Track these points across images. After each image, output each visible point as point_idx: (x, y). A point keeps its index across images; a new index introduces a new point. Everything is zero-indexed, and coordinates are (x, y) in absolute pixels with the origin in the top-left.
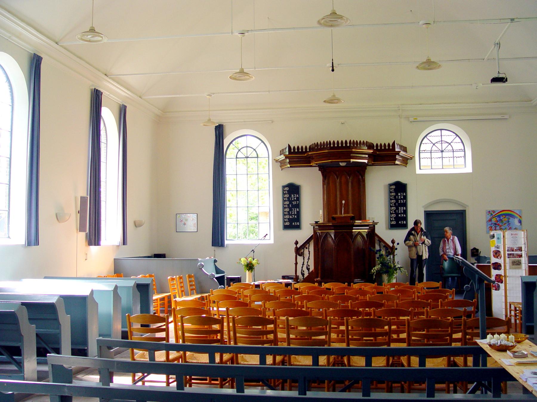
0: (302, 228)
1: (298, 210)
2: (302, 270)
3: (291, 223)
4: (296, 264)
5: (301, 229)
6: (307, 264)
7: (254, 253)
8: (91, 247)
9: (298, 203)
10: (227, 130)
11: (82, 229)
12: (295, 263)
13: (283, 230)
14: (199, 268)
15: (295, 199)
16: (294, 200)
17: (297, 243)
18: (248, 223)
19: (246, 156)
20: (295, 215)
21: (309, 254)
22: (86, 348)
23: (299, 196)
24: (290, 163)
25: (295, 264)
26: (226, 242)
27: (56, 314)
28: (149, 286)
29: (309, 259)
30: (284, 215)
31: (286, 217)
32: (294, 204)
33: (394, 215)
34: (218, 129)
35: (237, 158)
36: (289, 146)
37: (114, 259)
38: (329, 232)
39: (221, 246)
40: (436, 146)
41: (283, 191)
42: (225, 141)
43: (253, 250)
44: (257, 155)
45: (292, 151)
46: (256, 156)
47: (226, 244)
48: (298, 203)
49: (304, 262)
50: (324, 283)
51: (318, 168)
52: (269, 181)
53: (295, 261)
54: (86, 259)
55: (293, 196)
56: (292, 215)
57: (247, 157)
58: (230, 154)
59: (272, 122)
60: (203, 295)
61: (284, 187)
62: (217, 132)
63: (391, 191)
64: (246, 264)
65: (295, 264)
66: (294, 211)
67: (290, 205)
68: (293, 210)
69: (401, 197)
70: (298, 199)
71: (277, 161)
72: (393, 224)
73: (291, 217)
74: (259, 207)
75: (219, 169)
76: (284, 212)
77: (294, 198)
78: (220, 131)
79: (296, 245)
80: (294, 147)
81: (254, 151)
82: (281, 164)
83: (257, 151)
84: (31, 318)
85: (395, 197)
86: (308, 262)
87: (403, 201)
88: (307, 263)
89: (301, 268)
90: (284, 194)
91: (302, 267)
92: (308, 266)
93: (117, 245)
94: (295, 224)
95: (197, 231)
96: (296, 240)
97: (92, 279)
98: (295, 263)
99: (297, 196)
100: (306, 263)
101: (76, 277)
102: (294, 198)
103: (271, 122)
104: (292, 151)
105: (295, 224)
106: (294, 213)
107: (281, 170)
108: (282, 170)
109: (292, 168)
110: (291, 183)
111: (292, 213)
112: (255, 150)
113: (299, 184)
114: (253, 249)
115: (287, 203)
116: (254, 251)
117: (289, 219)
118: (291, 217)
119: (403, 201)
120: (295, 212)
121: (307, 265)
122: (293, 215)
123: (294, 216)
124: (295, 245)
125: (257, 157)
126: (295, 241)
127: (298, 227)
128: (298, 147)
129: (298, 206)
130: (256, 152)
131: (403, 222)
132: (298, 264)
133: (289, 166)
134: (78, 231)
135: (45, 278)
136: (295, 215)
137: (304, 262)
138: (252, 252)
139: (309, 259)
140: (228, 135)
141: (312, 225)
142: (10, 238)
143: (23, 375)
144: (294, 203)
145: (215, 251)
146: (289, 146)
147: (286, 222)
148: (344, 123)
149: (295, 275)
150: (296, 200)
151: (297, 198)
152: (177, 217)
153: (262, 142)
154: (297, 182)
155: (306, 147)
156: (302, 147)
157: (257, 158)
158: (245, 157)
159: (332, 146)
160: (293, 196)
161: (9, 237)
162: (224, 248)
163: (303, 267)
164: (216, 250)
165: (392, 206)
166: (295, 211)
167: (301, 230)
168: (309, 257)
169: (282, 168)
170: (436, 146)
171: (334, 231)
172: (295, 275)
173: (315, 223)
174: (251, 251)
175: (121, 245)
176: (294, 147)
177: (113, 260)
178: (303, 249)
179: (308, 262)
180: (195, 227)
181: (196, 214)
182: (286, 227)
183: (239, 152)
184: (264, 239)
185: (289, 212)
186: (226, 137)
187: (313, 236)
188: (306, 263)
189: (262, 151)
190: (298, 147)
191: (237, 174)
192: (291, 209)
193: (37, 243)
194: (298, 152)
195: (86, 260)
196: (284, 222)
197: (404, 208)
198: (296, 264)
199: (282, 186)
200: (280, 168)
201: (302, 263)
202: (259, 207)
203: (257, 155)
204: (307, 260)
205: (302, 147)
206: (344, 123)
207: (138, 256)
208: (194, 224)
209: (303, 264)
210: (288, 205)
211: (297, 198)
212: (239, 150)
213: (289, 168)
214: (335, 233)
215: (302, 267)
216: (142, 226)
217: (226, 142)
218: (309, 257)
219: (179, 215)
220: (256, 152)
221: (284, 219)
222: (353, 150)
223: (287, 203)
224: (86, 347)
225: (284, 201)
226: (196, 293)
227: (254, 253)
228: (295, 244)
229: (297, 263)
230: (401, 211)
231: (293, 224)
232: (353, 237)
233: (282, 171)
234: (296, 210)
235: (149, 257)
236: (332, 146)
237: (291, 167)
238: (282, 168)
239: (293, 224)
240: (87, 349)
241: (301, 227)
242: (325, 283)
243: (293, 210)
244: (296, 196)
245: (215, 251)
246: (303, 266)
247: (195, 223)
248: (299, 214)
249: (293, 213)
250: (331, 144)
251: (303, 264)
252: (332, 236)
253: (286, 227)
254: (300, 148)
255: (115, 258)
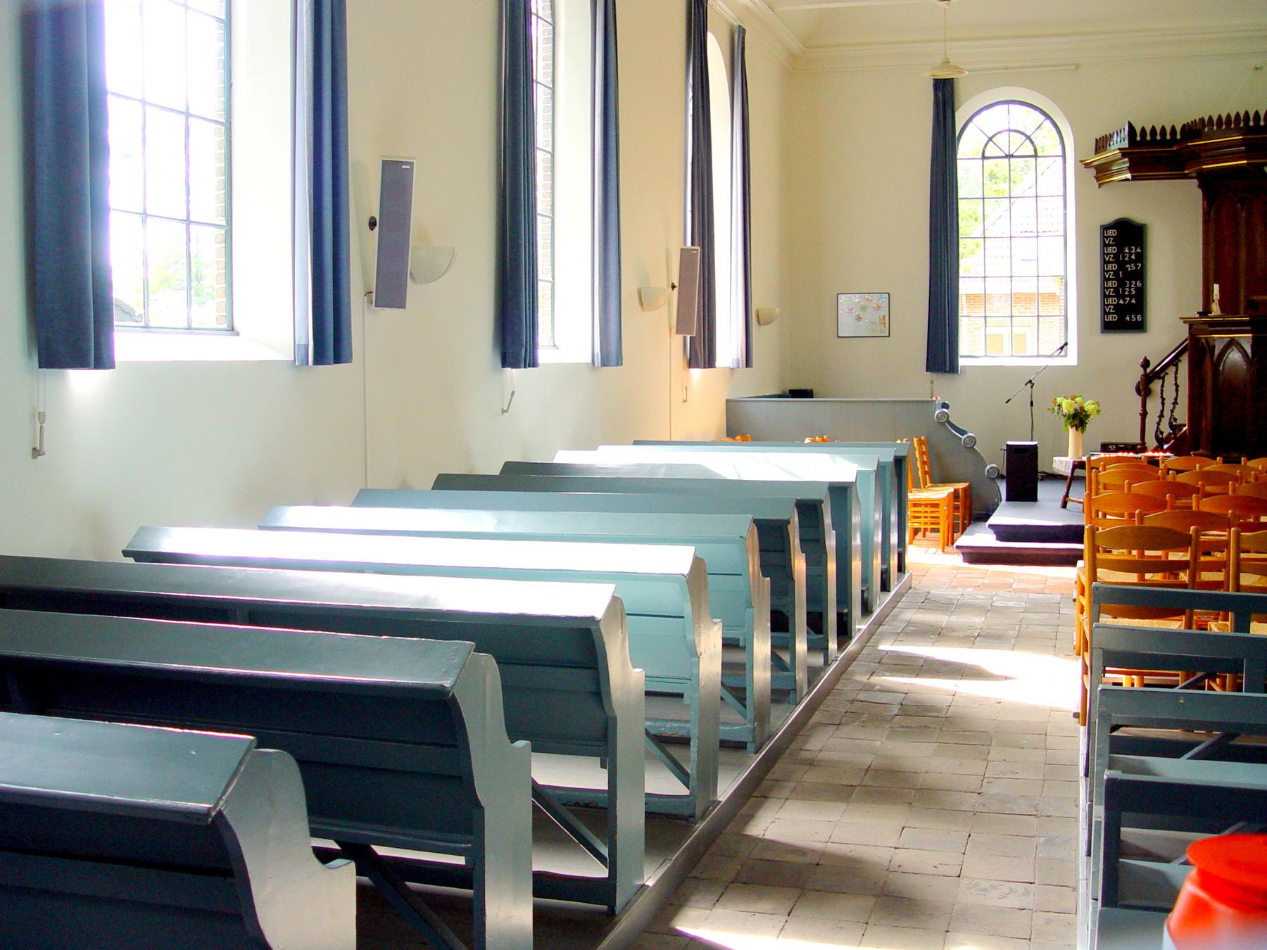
0: (1148, 330)
1: (1139, 284)
2: (1157, 431)
3: (1121, 318)
4: (1144, 415)
5: (1146, 332)
6: (1172, 415)
7: (1032, 387)
8: (691, 370)
9: (1139, 268)
10: (961, 90)
11: (681, 327)
12: (1141, 412)
13: (1102, 332)
14: (939, 422)
15: (1133, 257)
16: (1131, 261)
17: (1146, 363)
18: (985, 317)
19: (1008, 154)
20: (1131, 296)
21: (1177, 390)
22: (846, 611)
23: (1142, 251)
24: (1131, 169)
25: (1140, 414)
26: (962, 362)
27: (818, 527)
28: (903, 462)
29: (1175, 403)
30: (1105, 296)
31: (1110, 301)
32: (1129, 270)
33: (1114, 299)
34: (941, 86)
35: (984, 157)
36: (1131, 127)
37: (727, 401)
38: (1236, 339)
39: (949, 372)
40: (995, 144)
41: (1104, 237)
42: (957, 114)
43: (1030, 381)
44: (1035, 150)
45: (1138, 138)
46: (1033, 153)
47: (961, 366)
48: (1139, 268)
49: (1162, 411)
50: (1246, 459)
51: (1195, 182)
52: (1065, 215)
53: (1142, 407)
54: (685, 399)
55: (1127, 251)
56: (1123, 296)
57: (1009, 156)
58: (968, 146)
59: (1077, 68)
60: (956, 487)
61: (1105, 228)
62: (940, 94)
63: (1107, 242)
64: (1072, 412)
65: (1140, 414)
66: (1130, 288)
67: (1121, 273)
68: (1128, 286)
69: (1129, 258)
70: (1141, 258)
71: (1087, 165)
72: (1110, 321)
73: (1121, 302)
74: (1011, 277)
75: (944, 183)
76: (1104, 288)
77: (1131, 254)
78: (945, 94)
79: (1145, 370)
80: (1143, 130)
81: (1028, 141)
82: (1097, 173)
83: (1034, 140)
84: (805, 538)
85: (1116, 256)
86: (1172, 411)
87: (1137, 266)
88: (1170, 412)
89: (1156, 425)
90: (1105, 245)
91: (1158, 424)
92: (1172, 420)
93: (731, 367)
94: (1131, 318)
95: (838, 337)
96: (1144, 357)
97: (674, 445)
98: (1141, 412)
99: (1139, 250)
100: (1167, 414)
101: (668, 440)
102: (1131, 254)
103: (1074, 67)
104: (1138, 138)
105: (1131, 318)
106: (1130, 292)
107: (1098, 186)
108: (1099, 187)
109: (1137, 182)
110: (1122, 218)
111: (1124, 291)
112: (1028, 138)
113: (1143, 222)
114: (1031, 379)
115: (1113, 267)
116: (1033, 384)
117: (1117, 307)
118: (1121, 302)
119: (1137, 266)
120: (1132, 290)
121: (1171, 418)
122: (1127, 296)
123: (1128, 299)
124: (1142, 369)
125: (1036, 156)
126: (1142, 360)
127: (1139, 327)
128: (1153, 129)
129: (1140, 275)
130: (1032, 142)
131: (1136, 317)
132: (1148, 416)
133: (1129, 176)
134: (674, 330)
135: (636, 443)
136: (1131, 296)
137: (1162, 411)
138: (1029, 385)
139: (1175, 403)
140: (965, 102)
141: (1184, 322)
142: (558, 349)
143: (794, 674)
144: (1131, 267)
145: (932, 382)
146: (1131, 127)
147: (1109, 313)
148: (1261, 68)
149: (1140, 442)
150: (1135, 262)
151: (1137, 254)
152: (840, 301)
153: (1048, 117)
154: (1138, 217)
155: (1173, 129)
156: (1163, 129)
157: (1034, 159)
158: (1004, 155)
159: (1251, 124)
160: (1127, 251)
161: (555, 346)
162: (956, 375)
163: (1161, 423)
164: (935, 382)
165: (1109, 279)
166: (1131, 288)
167: (1146, 334)
168: (1176, 399)
169: (1100, 182)
170: (995, 144)
171: (1251, 335)
172: (1140, 442)
173: (1198, 316)
174: (1026, 384)
175: (743, 367)
176: (1143, 130)
177: (725, 402)
178: (1159, 378)
179: (1172, 411)
180: (885, 327)
181: (887, 295)
182: (1108, 327)
183: (990, 143)
184: (1058, 356)
185: (1116, 290)
186: (960, 107)
187: (1189, 347)
188: (1167, 414)
189: (1047, 139)
190: (1153, 129)
191: (1037, 197)
192: (1122, 284)
193: (619, 362)
194: (1154, 142)
195: (684, 401)
196: (1105, 313)
197: (1138, 284)
198: (1144, 415)
199: (1101, 226)
200: (1095, 181)
201: (1159, 414)
202: (1038, 276)
203: (1035, 150)
204: (1172, 406)
205: (1163, 129)
206: (1261, 68)
207: (762, 395)
208: (882, 317)
209: (1161, 416)
210: (1116, 273)
211: (1137, 254)
212: (990, 139)
213: (1127, 182)
214: (1254, 339)
215: (1158, 424)
216: (769, 323)
217: (960, 117)
218: (1176, 399)
219: (843, 296)
220: (1032, 142)
221: (1104, 305)
222: (1241, 137)
223: (1113, 267)
224: (847, 607)
225: (1105, 262)
226: (932, 483)
227: (1032, 387)
228: (1142, 366)
229: (1147, 413)
230: (1130, 290)
231: (1128, 318)
232: (1217, 352)
233: (1102, 188)
234: (1136, 285)
235: (780, 396)
236: (1251, 124)
237: (1134, 178)
238: (1100, 182)
239: (1128, 318)
240: (847, 613)
241: (1146, 328)
242: (1249, 459)
243: (1128, 286)
244: (1136, 249)
245: (932, 382)
246: (1160, 421)
247: (884, 316)
248: (1141, 294)
249: (1126, 293)
250: (1249, 120)
251: (1161, 416)
252: (1246, 349)
253: (1108, 327)
254: (1158, 131)
255: (729, 398)
